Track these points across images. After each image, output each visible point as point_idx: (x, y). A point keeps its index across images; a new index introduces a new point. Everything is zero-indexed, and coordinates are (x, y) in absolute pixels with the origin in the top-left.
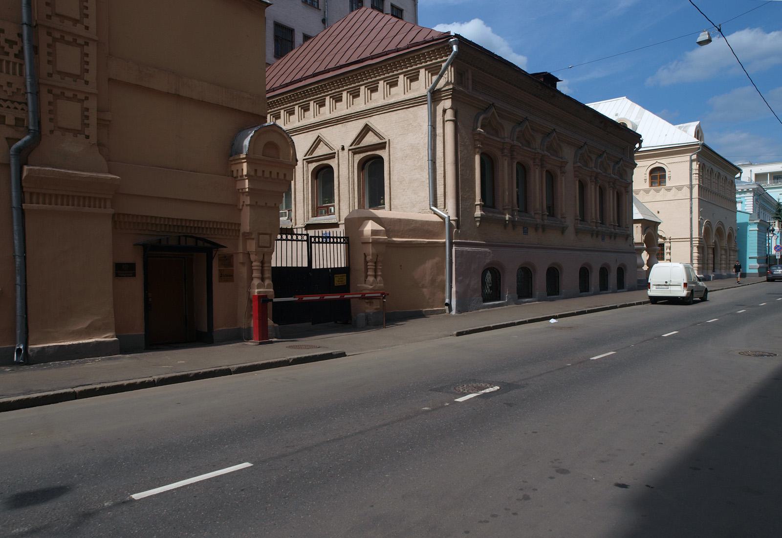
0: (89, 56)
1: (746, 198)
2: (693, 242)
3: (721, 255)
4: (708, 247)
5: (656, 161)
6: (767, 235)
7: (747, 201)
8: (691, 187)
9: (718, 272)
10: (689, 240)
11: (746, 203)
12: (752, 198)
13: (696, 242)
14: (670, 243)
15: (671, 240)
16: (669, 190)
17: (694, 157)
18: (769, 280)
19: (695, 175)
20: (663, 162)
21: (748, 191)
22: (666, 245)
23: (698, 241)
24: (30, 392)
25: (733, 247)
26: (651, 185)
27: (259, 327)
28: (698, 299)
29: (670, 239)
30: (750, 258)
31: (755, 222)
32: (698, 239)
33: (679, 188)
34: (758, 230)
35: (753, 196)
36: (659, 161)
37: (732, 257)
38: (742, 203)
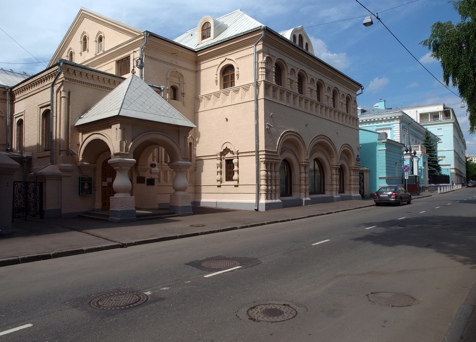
1: (394, 125)
2: (260, 157)
4: (350, 169)
6: (402, 157)
7: (395, 127)
8: (257, 86)
9: (347, 193)
10: (254, 154)
11: (394, 129)
12: (399, 125)
13: (262, 157)
14: (238, 158)
15: (239, 155)
16: (237, 91)
17: (260, 47)
18: (378, 204)
20: (233, 58)
21: (395, 118)
22: (235, 161)
23: (265, 154)
24: (145, 238)
28: (406, 203)
29: (238, 154)
30: (380, 178)
31: (383, 141)
32: (264, 153)
33: (246, 88)
34: (386, 150)
35: (400, 124)
36: (228, 57)
38: (391, 129)
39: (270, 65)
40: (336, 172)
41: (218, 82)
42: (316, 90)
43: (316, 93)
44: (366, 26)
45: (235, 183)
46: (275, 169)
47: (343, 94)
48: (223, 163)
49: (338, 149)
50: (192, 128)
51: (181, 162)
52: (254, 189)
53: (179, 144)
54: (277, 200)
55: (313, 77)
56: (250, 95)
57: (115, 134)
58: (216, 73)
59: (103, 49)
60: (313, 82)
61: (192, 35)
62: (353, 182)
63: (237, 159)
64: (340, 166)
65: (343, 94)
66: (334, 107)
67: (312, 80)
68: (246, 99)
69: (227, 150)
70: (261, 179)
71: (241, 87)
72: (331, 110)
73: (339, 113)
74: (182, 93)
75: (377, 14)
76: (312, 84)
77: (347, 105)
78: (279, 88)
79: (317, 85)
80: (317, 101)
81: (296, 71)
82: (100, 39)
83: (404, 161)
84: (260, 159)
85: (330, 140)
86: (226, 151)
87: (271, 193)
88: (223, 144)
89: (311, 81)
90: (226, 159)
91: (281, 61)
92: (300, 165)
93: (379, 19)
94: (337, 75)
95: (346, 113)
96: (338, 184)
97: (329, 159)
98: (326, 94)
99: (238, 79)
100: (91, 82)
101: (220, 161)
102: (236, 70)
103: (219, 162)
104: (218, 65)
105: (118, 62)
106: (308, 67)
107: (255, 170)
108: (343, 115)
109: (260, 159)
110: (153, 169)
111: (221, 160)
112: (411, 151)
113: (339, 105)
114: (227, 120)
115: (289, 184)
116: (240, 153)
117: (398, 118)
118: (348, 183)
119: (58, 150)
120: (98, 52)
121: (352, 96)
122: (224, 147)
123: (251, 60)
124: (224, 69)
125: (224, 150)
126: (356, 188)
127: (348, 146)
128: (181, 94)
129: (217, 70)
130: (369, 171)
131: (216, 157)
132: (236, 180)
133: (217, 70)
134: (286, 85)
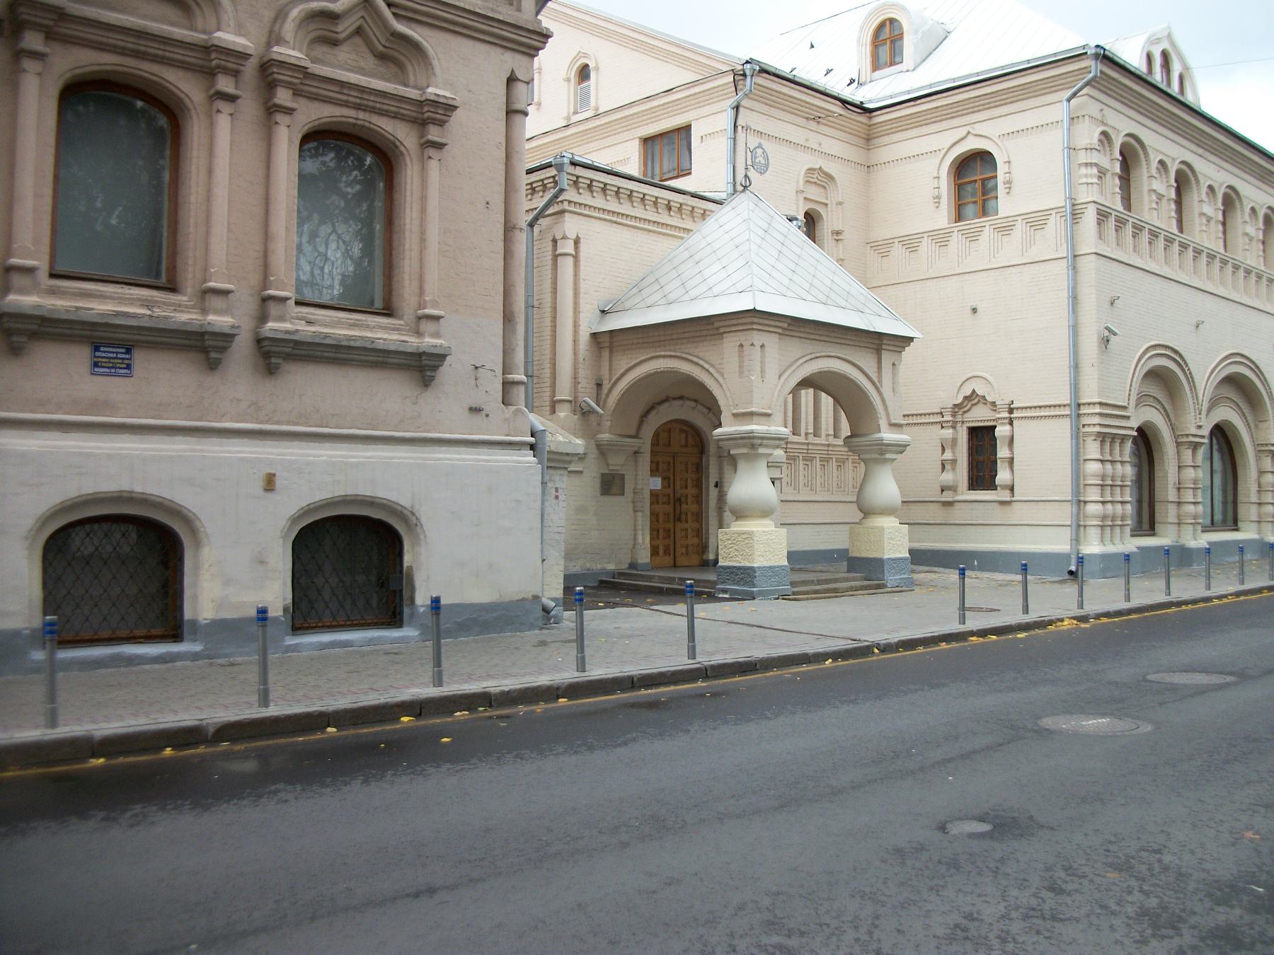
0: (268, 495)
3: (1261, 473)
5: (968, 128)
14: (1011, 423)
16: (1005, 229)
19: (1083, 171)
22: (1002, 431)
25: (1193, 431)
26: (959, 217)
27: (131, 492)
29: (1011, 411)
33: (1036, 221)
36: (979, 129)
37: (1190, 473)
40: (1193, 460)
43: (1117, 181)
46: (1102, 454)
47: (1161, 162)
48: (959, 437)
49: (1201, 383)
51: (888, 436)
52: (1065, 514)
56: (1052, 240)
57: (737, 359)
59: (593, 103)
62: (1191, 492)
63: (1008, 427)
64: (1140, 430)
65: (1161, 162)
66: (1181, 231)
67: (1103, 137)
68: (1033, 254)
71: (1019, 218)
72: (1169, 241)
73: (1198, 252)
77: (1179, 203)
79: (1121, 154)
80: (1121, 208)
82: (584, 73)
85: (1256, 369)
92: (1178, 444)
95: (1222, 251)
97: (1252, 426)
98: (1204, 207)
100: (651, 215)
101: (951, 431)
103: (948, 433)
104: (943, 152)
105: (646, 141)
106: (1200, 151)
107: (1069, 458)
108: (1211, 257)
111: (954, 427)
113: (1239, 241)
114: (974, 310)
118: (1172, 496)
119: (548, 399)
120: (576, 113)
123: (1055, 140)
125: (966, 398)
126: (1114, 518)
131: (939, 419)
132: (1004, 487)
134: (1146, 208)
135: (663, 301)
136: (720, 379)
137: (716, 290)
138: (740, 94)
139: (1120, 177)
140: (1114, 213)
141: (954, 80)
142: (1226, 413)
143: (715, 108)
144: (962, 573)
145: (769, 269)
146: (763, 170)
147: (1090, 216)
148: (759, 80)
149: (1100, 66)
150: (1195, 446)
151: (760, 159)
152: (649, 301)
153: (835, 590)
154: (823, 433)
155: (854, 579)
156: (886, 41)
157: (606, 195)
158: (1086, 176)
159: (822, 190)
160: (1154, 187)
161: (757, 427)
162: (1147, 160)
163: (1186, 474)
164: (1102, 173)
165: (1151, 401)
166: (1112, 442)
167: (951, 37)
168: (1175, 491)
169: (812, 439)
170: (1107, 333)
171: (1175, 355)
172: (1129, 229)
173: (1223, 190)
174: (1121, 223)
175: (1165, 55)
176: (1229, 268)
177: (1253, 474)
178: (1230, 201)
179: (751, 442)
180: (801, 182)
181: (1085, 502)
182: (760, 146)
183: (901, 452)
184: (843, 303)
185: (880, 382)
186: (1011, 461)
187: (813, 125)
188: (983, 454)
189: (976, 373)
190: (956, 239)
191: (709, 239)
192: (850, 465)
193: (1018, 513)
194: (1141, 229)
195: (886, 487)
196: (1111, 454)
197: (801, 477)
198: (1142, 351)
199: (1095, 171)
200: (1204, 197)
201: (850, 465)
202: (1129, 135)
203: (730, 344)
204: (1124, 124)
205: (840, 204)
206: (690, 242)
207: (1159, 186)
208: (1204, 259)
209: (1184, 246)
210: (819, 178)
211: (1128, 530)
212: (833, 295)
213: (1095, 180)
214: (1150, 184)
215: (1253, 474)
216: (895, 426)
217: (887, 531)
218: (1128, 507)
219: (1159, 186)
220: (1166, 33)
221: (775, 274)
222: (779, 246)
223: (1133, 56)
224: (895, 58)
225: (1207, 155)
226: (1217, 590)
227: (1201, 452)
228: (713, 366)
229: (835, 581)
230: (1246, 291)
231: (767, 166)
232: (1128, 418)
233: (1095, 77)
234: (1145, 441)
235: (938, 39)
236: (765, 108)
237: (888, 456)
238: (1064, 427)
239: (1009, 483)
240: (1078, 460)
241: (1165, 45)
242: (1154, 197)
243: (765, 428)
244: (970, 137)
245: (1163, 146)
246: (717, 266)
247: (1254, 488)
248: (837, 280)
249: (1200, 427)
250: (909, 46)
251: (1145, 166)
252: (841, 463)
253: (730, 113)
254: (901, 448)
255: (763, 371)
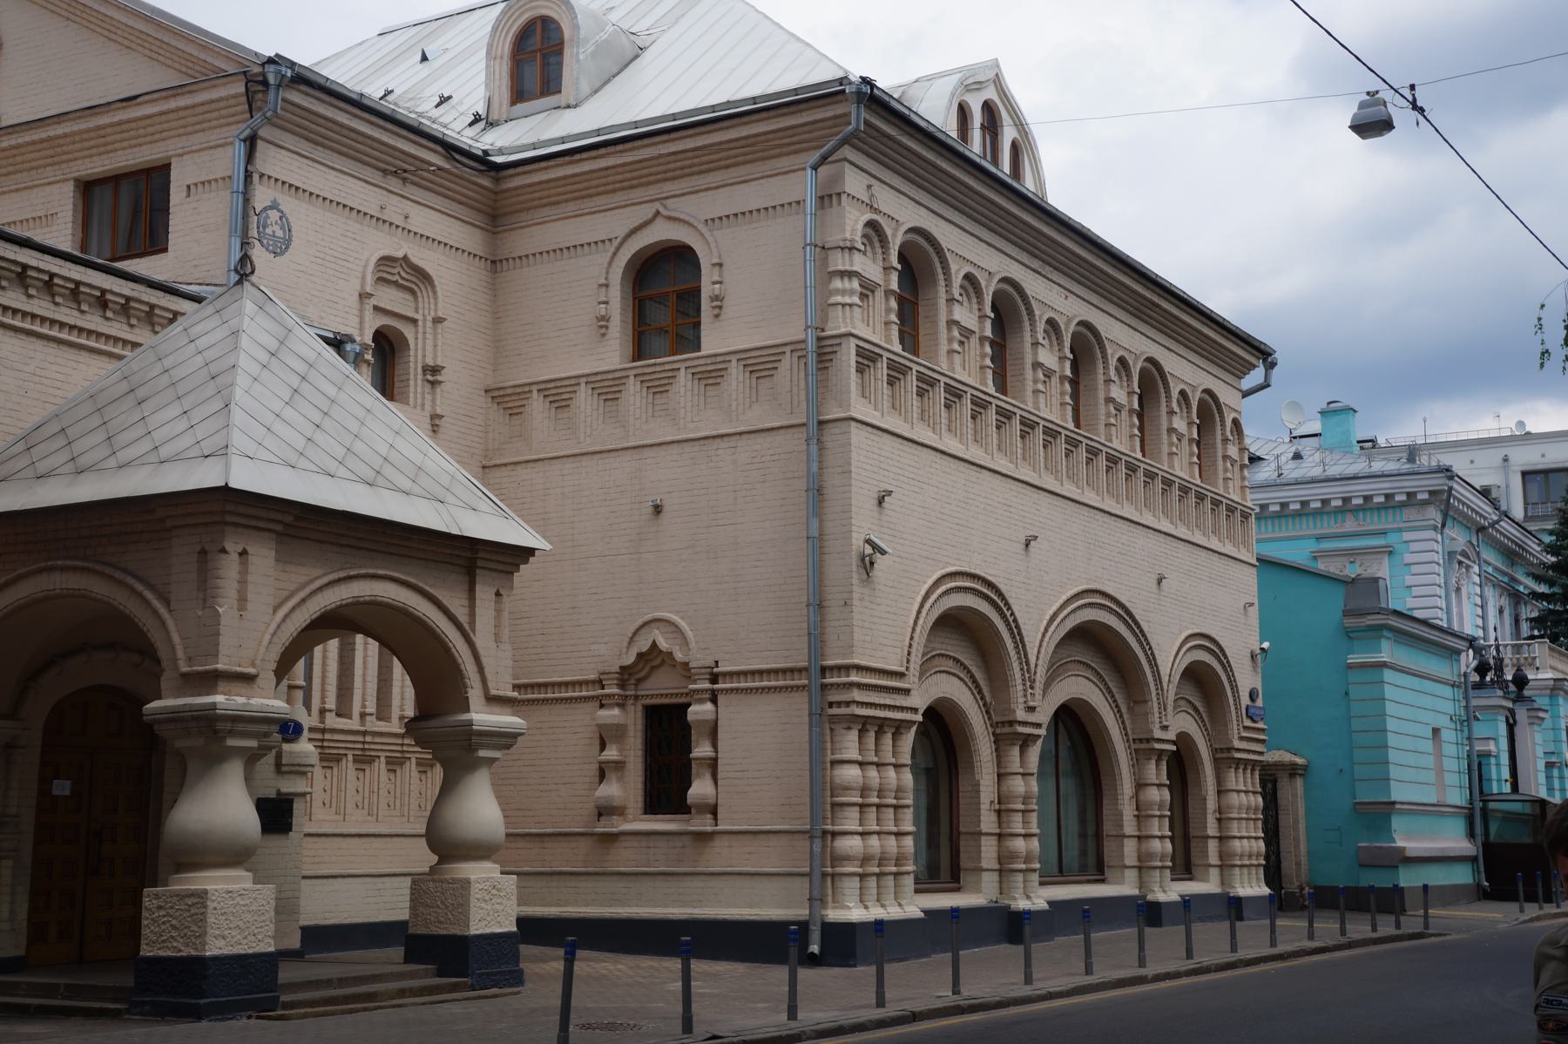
5: (657, 205)
11: (1408, 558)
16: (711, 376)
22: (699, 711)
26: (639, 353)
29: (714, 679)
33: (760, 364)
39: (874, 260)
41: (611, 324)
42: (988, 333)
44: (1363, 137)
45: (702, 824)
47: (1122, 360)
50: (530, 552)
51: (482, 717)
53: (474, 631)
54: (890, 909)
55: (1052, 314)
58: (603, 281)
60: (877, 244)
61: (424, 58)
62: (1018, 817)
63: (709, 706)
66: (1002, 387)
67: (966, 283)
69: (652, 658)
70: (833, 805)
71: (734, 358)
72: (1131, 468)
73: (1168, 483)
74: (426, 369)
75: (1412, 87)
76: (874, 253)
77: (1075, 382)
78: (915, 367)
79: (994, 308)
80: (898, 348)
81: (983, 284)
83: (1475, 724)
84: (831, 705)
86: (647, 661)
87: (1221, 867)
88: (632, 629)
89: (864, 236)
90: (648, 701)
91: (921, 241)
93: (1421, 110)
94: (1156, 299)
95: (1071, 426)
96: (911, 828)
99: (717, 316)
102: (707, 276)
103: (612, 715)
104: (616, 243)
105: (87, 188)
106: (1036, 264)
108: (1185, 490)
109: (831, 705)
110: (286, 747)
112: (1499, 668)
114: (658, 509)
115: (944, 828)
116: (725, 674)
117: (1425, 503)
121: (1166, 369)
122: (643, 645)
124: (644, 264)
125: (640, 656)
127: (953, 584)
128: (420, 370)
129: (610, 264)
130: (1305, 768)
133: (610, 264)
135: (70, 467)
136: (163, 611)
137: (165, 452)
138: (257, 115)
139: (993, 343)
140: (886, 355)
141: (636, 124)
142: (1080, 687)
143: (214, 137)
144: (570, 961)
145: (269, 418)
146: (281, 248)
147: (848, 356)
148: (295, 97)
149: (864, 114)
150: (1026, 741)
151: (274, 229)
152: (42, 467)
153: (370, 997)
154: (395, 713)
155: (412, 975)
156: (536, 58)
157: (26, 287)
158: (843, 292)
159: (408, 296)
160: (956, 317)
161: (223, 700)
162: (1104, 355)
163: (1010, 790)
164: (868, 289)
165: (949, 665)
166: (879, 733)
167: (646, 57)
168: (994, 817)
169: (332, 721)
170: (868, 550)
171: (990, 590)
172: (912, 382)
173: (1198, 395)
174: (1073, 443)
175: (988, 107)
176: (1082, 454)
177: (1127, 788)
178: (1007, 313)
179: (212, 726)
180: (369, 279)
181: (834, 834)
182: (274, 206)
183: (508, 747)
184: (406, 484)
185: (472, 622)
186: (713, 764)
187: (394, 183)
188: (669, 754)
189: (649, 617)
190: (633, 388)
191: (167, 363)
192: (411, 767)
193: (721, 855)
194: (932, 383)
195: (481, 808)
196: (877, 752)
197: (351, 792)
198: (930, 582)
199: (855, 284)
200: (1112, 374)
201: (411, 767)
202: (913, 230)
203: (466, 602)
204: (904, 212)
205: (438, 321)
206: (135, 366)
207: (965, 315)
208: (1039, 436)
209: (1151, 476)
210: (403, 274)
211: (909, 881)
212: (388, 471)
213: (856, 300)
214: (950, 312)
215: (1127, 788)
216: (493, 700)
217: (475, 888)
218: (909, 842)
219: (965, 315)
220: (992, 75)
221: (279, 427)
222: (295, 381)
223: (936, 111)
224: (550, 84)
225: (1047, 270)
226: (1047, 982)
227: (1034, 753)
228: (152, 588)
229: (375, 978)
230: (1050, 468)
231: (288, 243)
232: (907, 692)
233: (857, 129)
234: (941, 734)
235: (626, 55)
236: (304, 147)
237: (482, 753)
238: (798, 706)
239: (712, 801)
240: (821, 763)
241: (990, 94)
242: (956, 333)
243: (241, 700)
244: (659, 221)
245: (970, 252)
246: (175, 410)
247: (1128, 812)
248: (400, 444)
249: (1031, 709)
250: (577, 66)
251: (1027, 324)
252: (395, 763)
253: (240, 149)
254: (505, 739)
255: (242, 600)
